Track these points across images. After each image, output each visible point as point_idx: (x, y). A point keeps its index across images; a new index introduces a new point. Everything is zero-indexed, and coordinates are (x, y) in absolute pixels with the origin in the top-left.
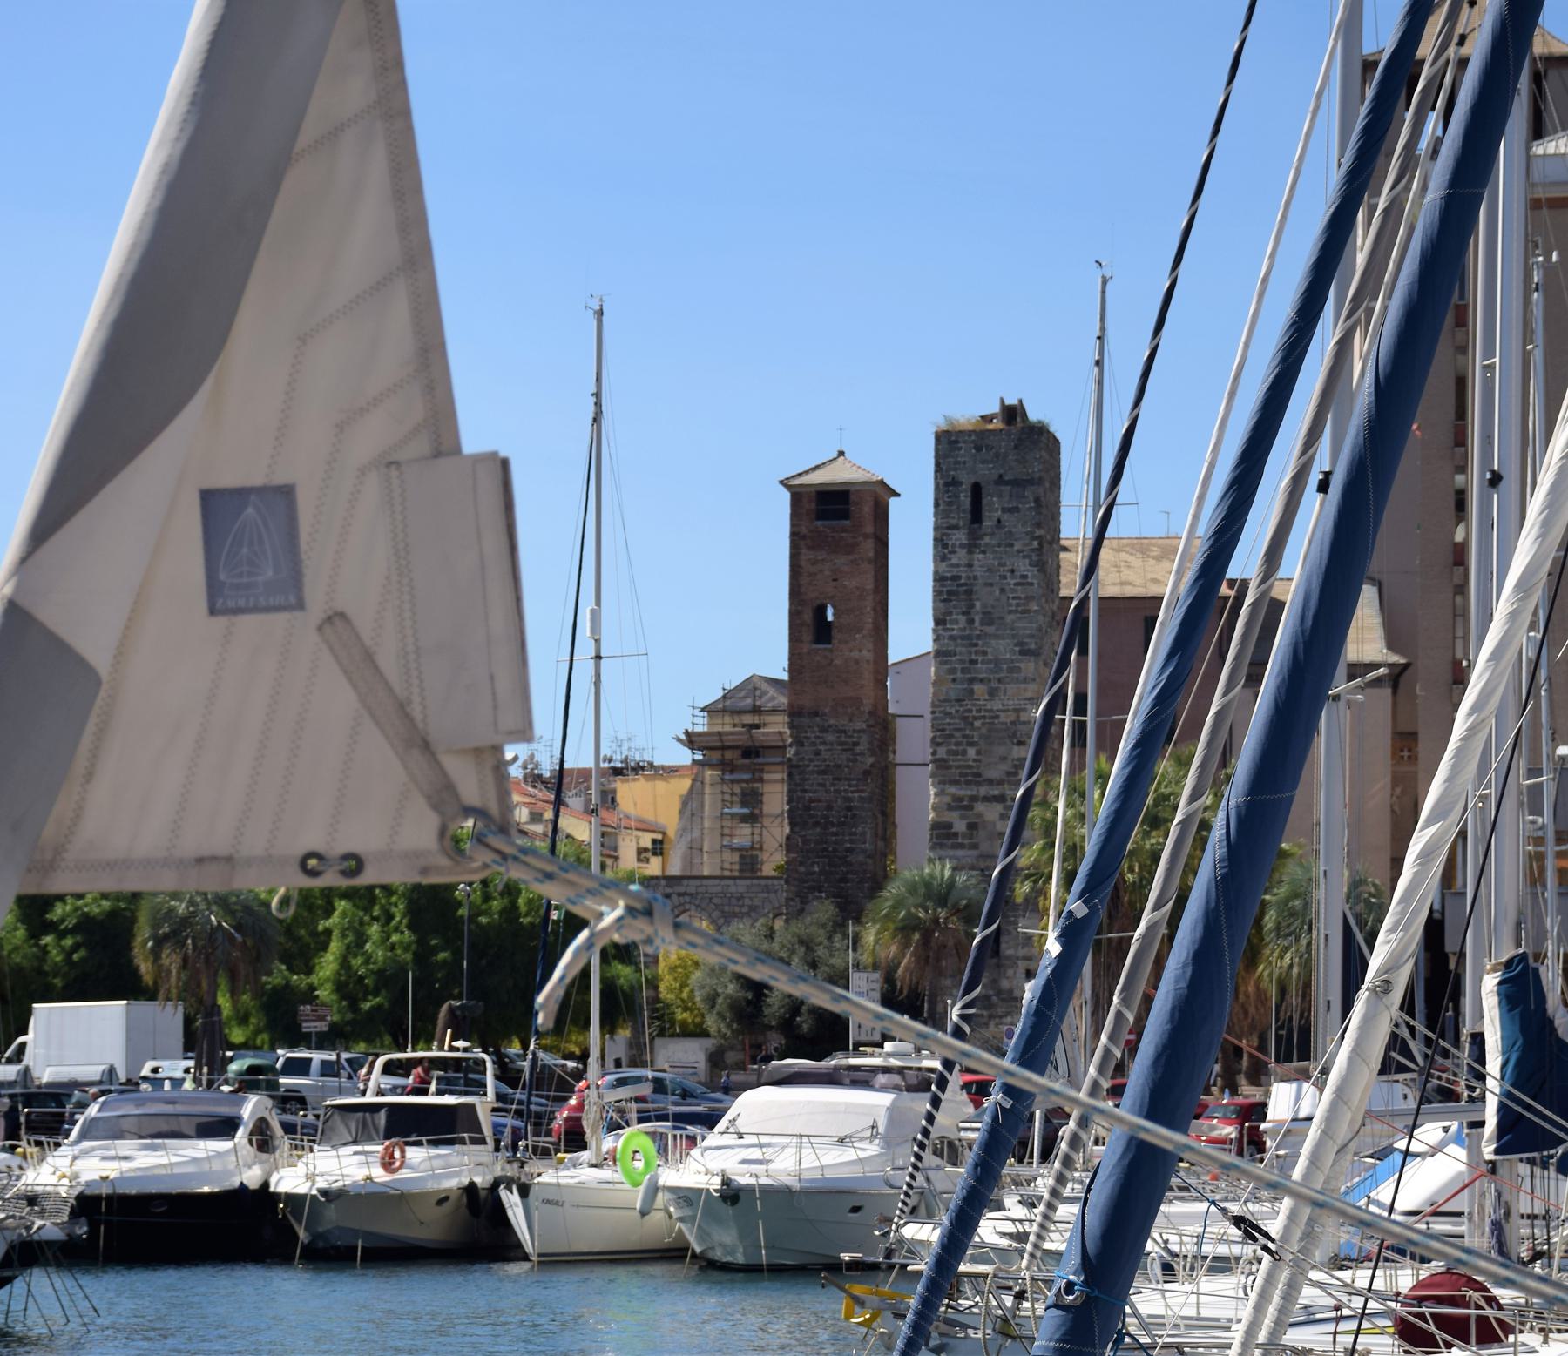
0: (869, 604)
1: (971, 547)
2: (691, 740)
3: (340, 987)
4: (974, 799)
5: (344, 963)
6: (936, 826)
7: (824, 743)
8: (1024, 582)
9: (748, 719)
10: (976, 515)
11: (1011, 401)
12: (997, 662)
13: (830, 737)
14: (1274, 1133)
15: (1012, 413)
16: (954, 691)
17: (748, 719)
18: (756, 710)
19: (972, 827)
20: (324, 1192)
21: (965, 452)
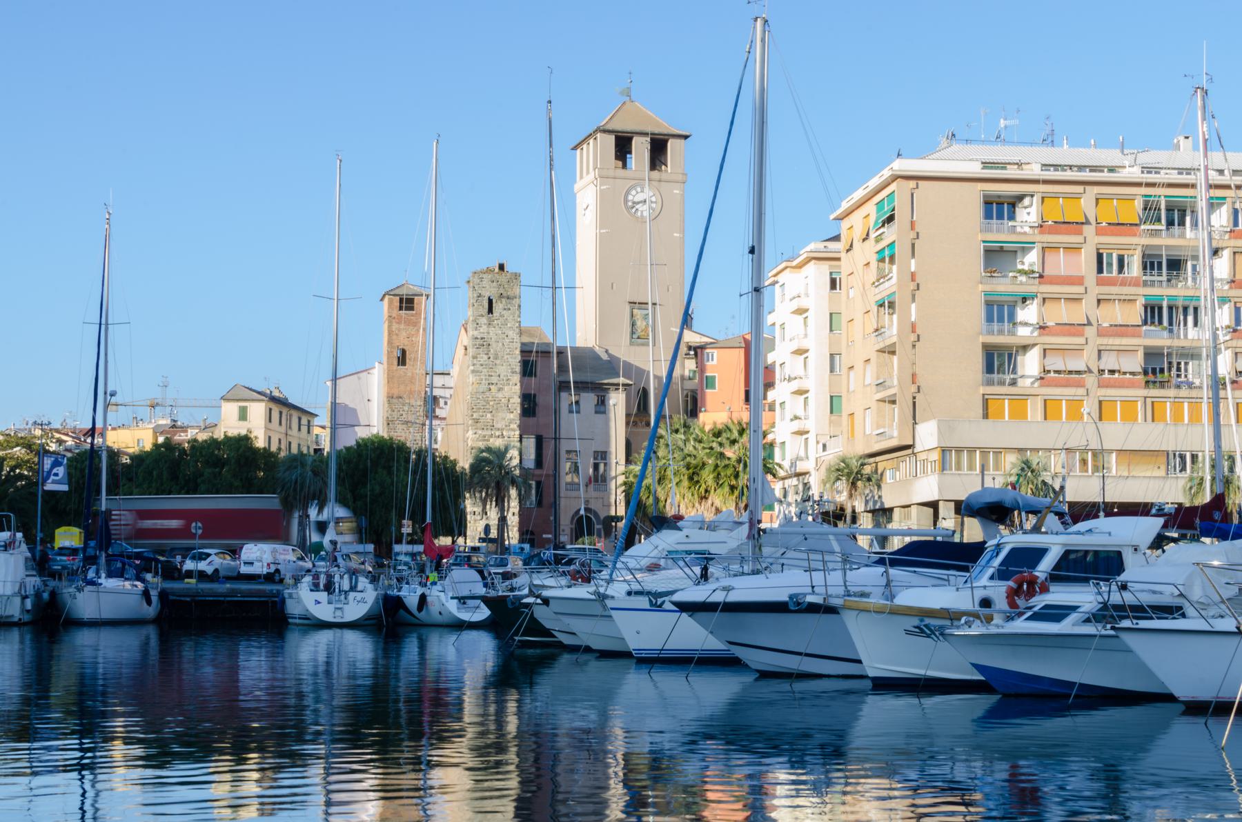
13: (406, 408)
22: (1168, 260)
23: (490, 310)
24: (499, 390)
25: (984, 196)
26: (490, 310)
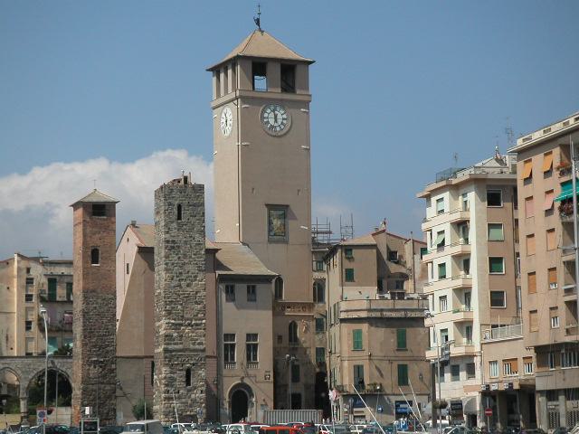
4: (181, 325)
7: (97, 303)
13: (99, 301)
22: (406, 365)
23: (179, 217)
24: (188, 285)
25: (113, 204)
26: (179, 217)
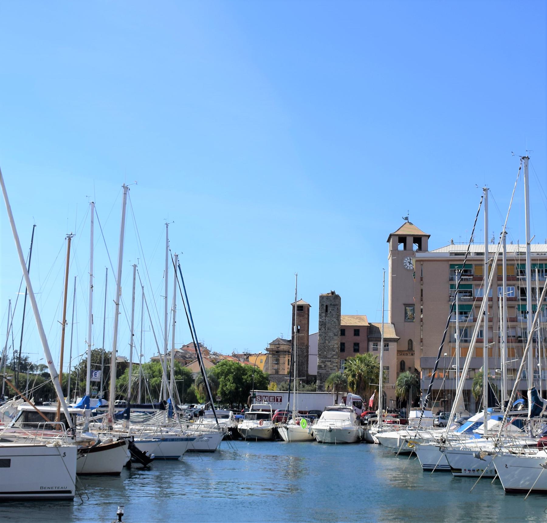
0: (306, 326)
1: (326, 316)
2: (267, 349)
3: (222, 393)
5: (222, 389)
6: (319, 366)
8: (335, 323)
9: (277, 346)
10: (327, 311)
11: (333, 291)
12: (330, 337)
14: (410, 420)
15: (333, 293)
16: (322, 342)
17: (277, 346)
18: (279, 344)
19: (325, 366)
20: (250, 429)
21: (325, 300)
